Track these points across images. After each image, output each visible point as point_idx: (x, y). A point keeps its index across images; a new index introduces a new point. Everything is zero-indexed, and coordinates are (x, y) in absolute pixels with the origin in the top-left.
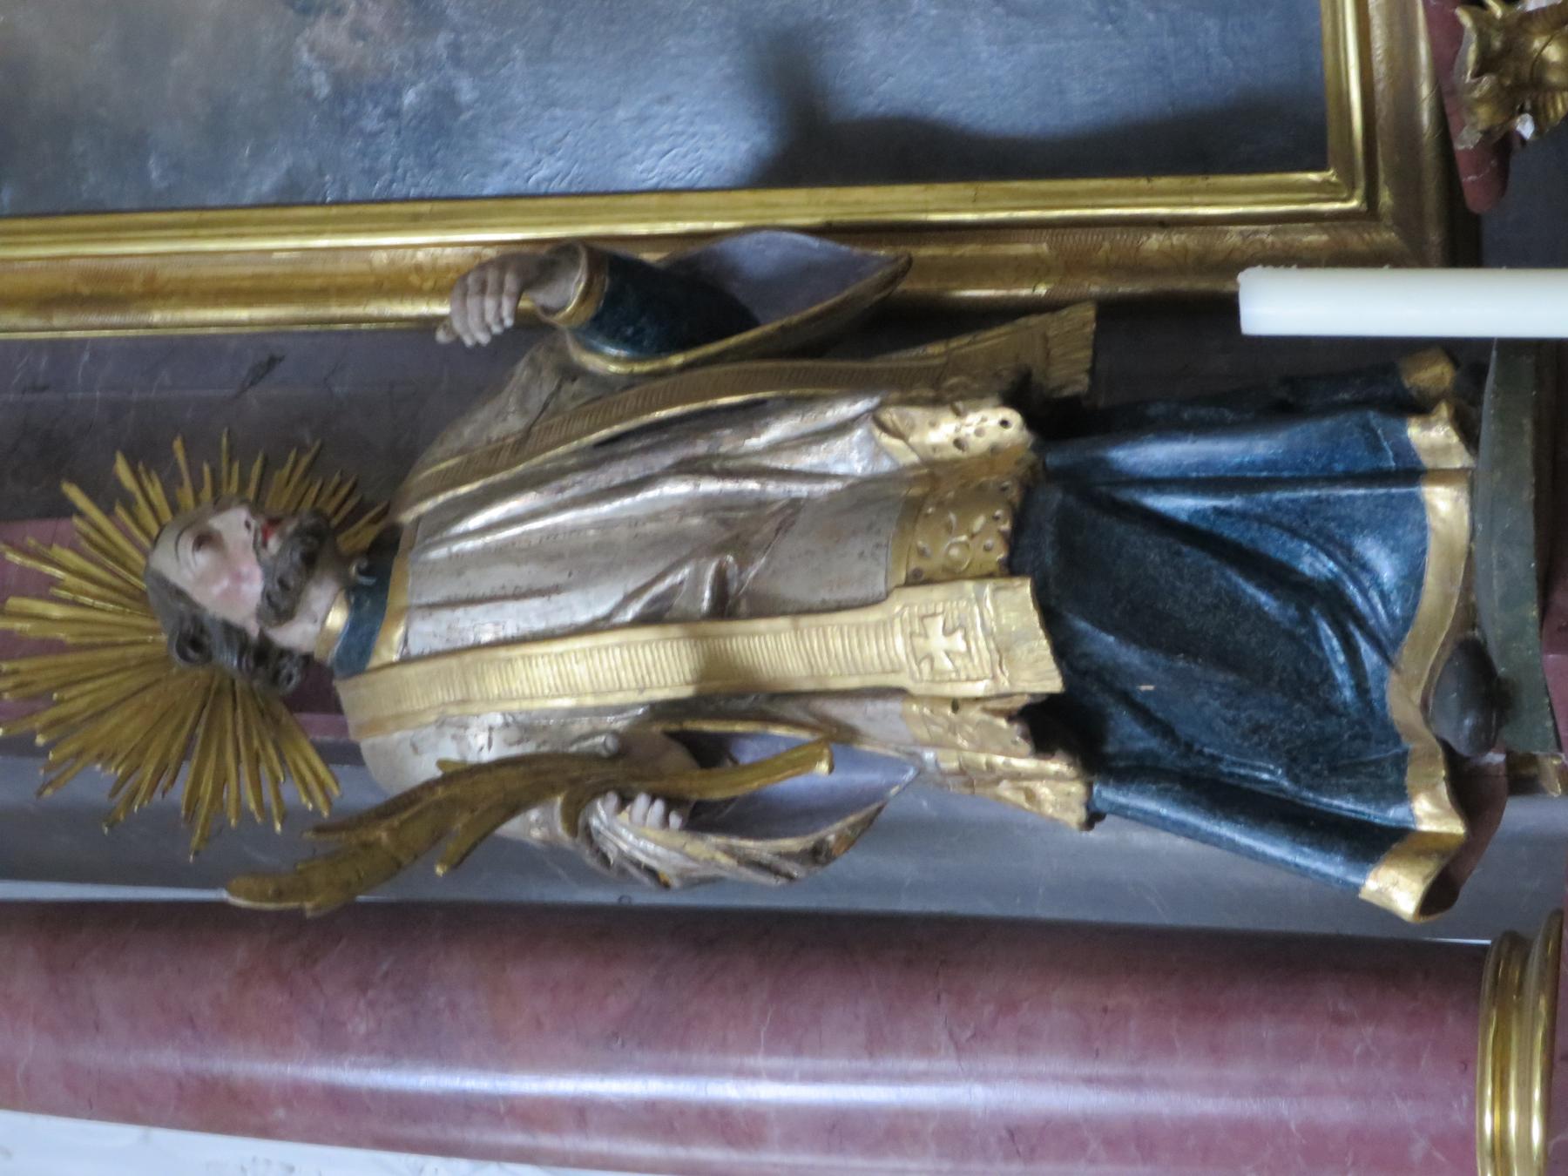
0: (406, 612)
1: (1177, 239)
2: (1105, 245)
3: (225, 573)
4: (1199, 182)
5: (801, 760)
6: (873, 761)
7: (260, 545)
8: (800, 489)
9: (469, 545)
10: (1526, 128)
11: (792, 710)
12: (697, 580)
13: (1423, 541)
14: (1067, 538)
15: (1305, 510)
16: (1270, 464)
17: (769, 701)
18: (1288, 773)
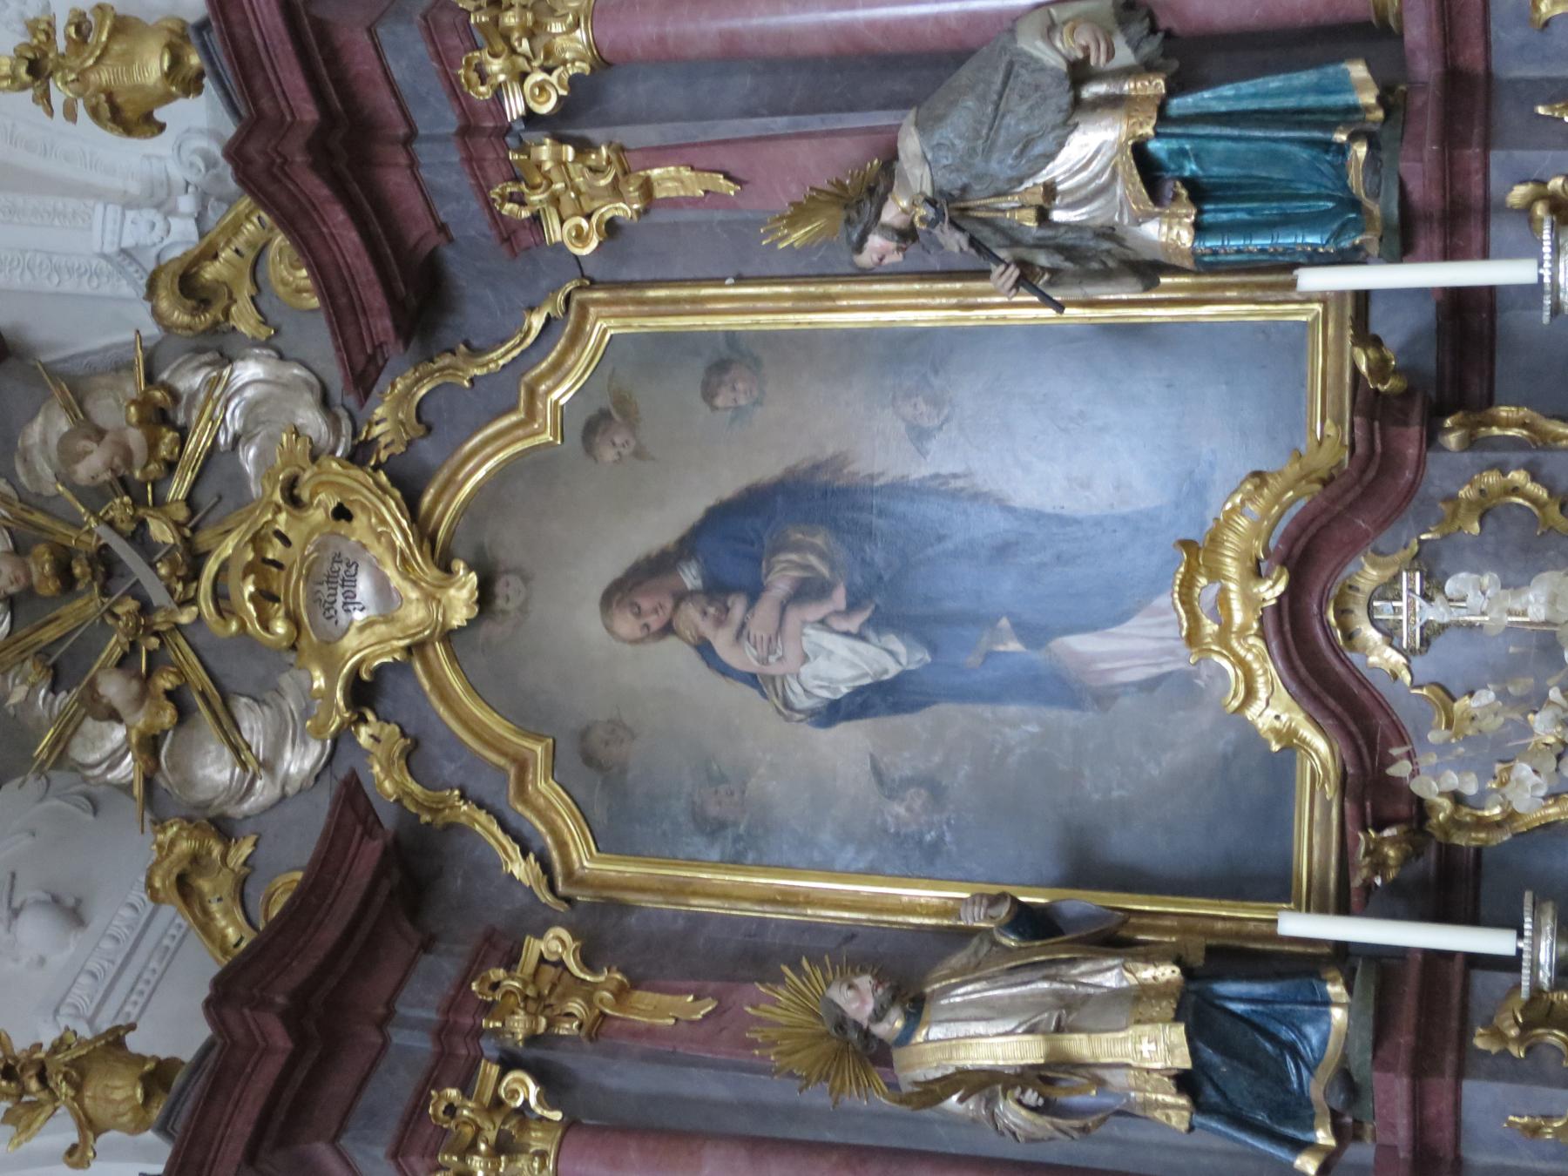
0: (929, 1024)
1: (1229, 925)
2: (1200, 924)
3: (857, 999)
4: (1240, 904)
5: (1081, 1090)
6: (1111, 1094)
7: (874, 990)
8: (1091, 991)
9: (958, 999)
10: (1378, 881)
11: (1082, 1071)
12: (1050, 1018)
13: (1329, 1030)
14: (1195, 1010)
15: (1285, 1014)
16: (1274, 995)
17: (1073, 1066)
18: (1270, 1118)
